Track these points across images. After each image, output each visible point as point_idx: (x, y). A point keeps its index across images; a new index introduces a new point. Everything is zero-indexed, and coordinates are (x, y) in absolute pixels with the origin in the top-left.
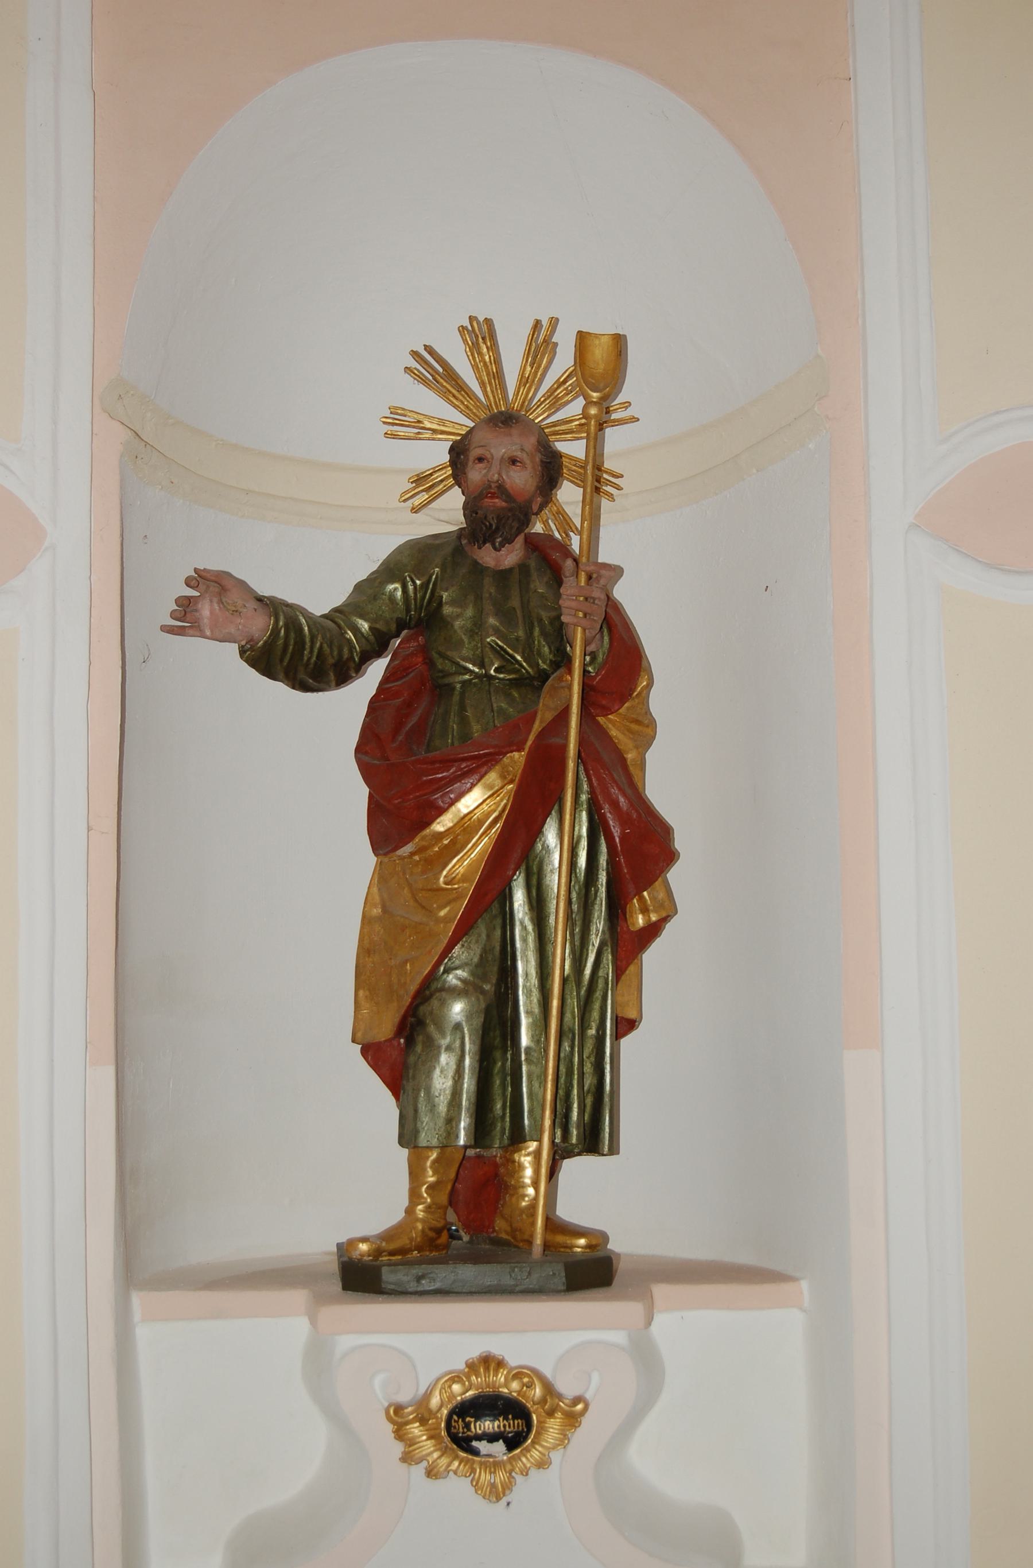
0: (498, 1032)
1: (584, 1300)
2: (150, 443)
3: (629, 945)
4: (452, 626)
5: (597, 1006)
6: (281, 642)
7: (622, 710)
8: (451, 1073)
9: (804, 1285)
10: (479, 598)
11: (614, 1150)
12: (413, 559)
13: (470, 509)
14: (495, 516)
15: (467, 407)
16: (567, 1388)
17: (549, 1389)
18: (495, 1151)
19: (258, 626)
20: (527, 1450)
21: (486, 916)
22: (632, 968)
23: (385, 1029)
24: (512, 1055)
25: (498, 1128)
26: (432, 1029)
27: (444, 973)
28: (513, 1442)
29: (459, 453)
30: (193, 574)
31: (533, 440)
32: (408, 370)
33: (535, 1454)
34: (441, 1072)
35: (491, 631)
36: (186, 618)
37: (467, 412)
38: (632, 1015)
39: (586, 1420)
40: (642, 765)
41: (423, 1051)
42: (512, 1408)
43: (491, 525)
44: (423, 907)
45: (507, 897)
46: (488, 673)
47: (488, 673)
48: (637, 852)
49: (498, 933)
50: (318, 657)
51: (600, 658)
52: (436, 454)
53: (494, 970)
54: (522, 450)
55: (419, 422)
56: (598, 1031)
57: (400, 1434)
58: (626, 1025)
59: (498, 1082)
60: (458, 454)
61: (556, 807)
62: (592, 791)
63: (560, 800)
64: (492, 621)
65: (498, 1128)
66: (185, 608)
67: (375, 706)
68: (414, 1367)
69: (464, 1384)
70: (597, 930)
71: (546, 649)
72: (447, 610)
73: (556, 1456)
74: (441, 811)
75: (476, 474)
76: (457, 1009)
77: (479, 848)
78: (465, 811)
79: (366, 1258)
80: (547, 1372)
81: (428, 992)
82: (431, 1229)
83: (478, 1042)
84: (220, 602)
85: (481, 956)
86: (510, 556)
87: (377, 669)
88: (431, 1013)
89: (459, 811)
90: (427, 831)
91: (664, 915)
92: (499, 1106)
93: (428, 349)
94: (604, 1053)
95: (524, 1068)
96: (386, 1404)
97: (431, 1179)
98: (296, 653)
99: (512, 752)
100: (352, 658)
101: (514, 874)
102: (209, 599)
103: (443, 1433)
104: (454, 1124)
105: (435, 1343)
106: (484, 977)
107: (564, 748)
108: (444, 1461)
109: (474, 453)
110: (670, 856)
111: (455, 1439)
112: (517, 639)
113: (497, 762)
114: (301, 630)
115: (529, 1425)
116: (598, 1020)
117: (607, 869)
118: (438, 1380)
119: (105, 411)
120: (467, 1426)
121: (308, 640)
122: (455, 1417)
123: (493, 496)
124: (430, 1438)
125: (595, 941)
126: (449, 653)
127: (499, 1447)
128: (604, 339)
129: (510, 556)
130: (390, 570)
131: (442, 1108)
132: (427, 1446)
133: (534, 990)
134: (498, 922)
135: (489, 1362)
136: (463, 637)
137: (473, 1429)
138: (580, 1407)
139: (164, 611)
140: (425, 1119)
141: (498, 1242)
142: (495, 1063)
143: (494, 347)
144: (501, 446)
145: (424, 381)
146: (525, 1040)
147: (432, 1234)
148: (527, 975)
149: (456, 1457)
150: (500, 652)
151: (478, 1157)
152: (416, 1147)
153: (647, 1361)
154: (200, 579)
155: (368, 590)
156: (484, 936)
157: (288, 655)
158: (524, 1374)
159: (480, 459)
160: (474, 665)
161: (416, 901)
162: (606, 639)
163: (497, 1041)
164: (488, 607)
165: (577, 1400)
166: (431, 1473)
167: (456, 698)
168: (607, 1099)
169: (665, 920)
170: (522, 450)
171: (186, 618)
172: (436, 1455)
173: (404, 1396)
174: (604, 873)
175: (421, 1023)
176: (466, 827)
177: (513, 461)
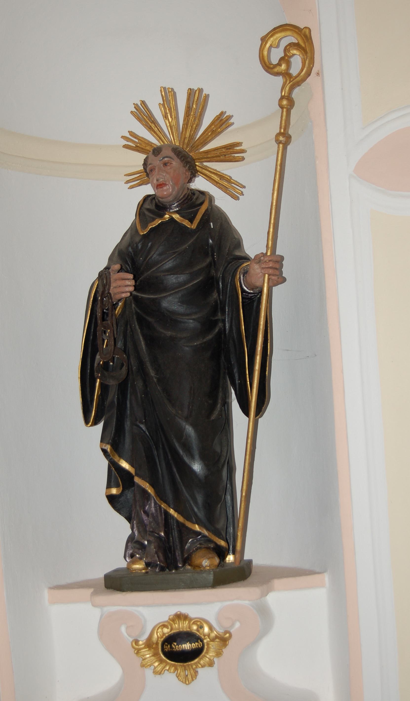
135: (180, 617)
138: (228, 635)
158: (200, 623)
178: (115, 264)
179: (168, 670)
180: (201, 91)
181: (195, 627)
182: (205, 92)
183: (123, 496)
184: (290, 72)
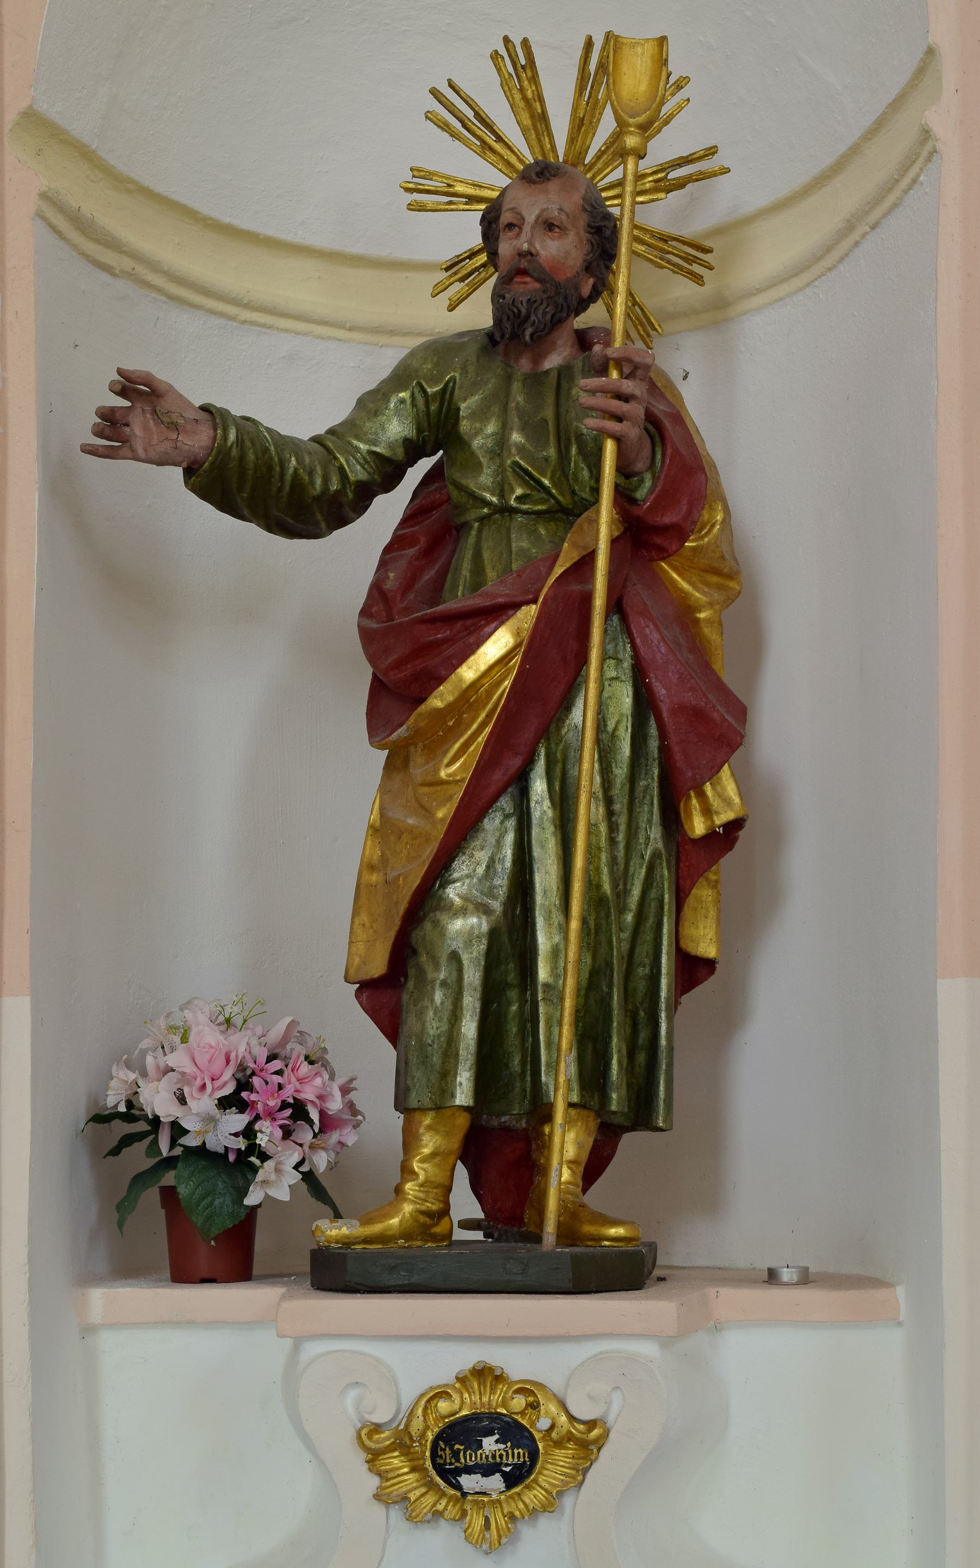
0: (511, 966)
1: (612, 1299)
4: (469, 446)
5: (648, 936)
8: (446, 1016)
9: (900, 1291)
10: (505, 409)
19: (199, 440)
23: (378, 966)
24: (531, 994)
25: (517, 1090)
26: (424, 958)
27: (439, 887)
29: (492, 224)
30: (118, 378)
31: (577, 198)
34: (435, 1013)
35: (514, 450)
41: (415, 988)
42: (513, 1432)
43: (520, 311)
44: (423, 807)
52: (466, 231)
56: (651, 970)
59: (515, 1030)
60: (490, 223)
65: (517, 1090)
66: (111, 423)
74: (441, 680)
88: (424, 939)
89: (461, 680)
90: (423, 708)
92: (517, 1061)
94: (659, 997)
95: (541, 1010)
96: (359, 1425)
98: (263, 485)
102: (135, 413)
103: (428, 1464)
104: (449, 1079)
105: (415, 1352)
106: (491, 894)
108: (430, 1499)
109: (506, 218)
111: (442, 1472)
112: (546, 460)
115: (534, 1455)
117: (660, 758)
118: (422, 1395)
120: (456, 1454)
122: (441, 1443)
124: (413, 1470)
126: (464, 482)
127: (496, 1482)
133: (554, 910)
134: (511, 824)
135: (485, 1375)
136: (482, 460)
137: (463, 1460)
138: (596, 1432)
139: (83, 427)
142: (510, 1003)
144: (532, 205)
146: (543, 974)
150: (524, 475)
159: (510, 226)
160: (492, 494)
161: (417, 801)
163: (512, 977)
164: (515, 420)
167: (472, 540)
172: (418, 1493)
174: (656, 764)
177: (549, 226)
178: (708, 621)
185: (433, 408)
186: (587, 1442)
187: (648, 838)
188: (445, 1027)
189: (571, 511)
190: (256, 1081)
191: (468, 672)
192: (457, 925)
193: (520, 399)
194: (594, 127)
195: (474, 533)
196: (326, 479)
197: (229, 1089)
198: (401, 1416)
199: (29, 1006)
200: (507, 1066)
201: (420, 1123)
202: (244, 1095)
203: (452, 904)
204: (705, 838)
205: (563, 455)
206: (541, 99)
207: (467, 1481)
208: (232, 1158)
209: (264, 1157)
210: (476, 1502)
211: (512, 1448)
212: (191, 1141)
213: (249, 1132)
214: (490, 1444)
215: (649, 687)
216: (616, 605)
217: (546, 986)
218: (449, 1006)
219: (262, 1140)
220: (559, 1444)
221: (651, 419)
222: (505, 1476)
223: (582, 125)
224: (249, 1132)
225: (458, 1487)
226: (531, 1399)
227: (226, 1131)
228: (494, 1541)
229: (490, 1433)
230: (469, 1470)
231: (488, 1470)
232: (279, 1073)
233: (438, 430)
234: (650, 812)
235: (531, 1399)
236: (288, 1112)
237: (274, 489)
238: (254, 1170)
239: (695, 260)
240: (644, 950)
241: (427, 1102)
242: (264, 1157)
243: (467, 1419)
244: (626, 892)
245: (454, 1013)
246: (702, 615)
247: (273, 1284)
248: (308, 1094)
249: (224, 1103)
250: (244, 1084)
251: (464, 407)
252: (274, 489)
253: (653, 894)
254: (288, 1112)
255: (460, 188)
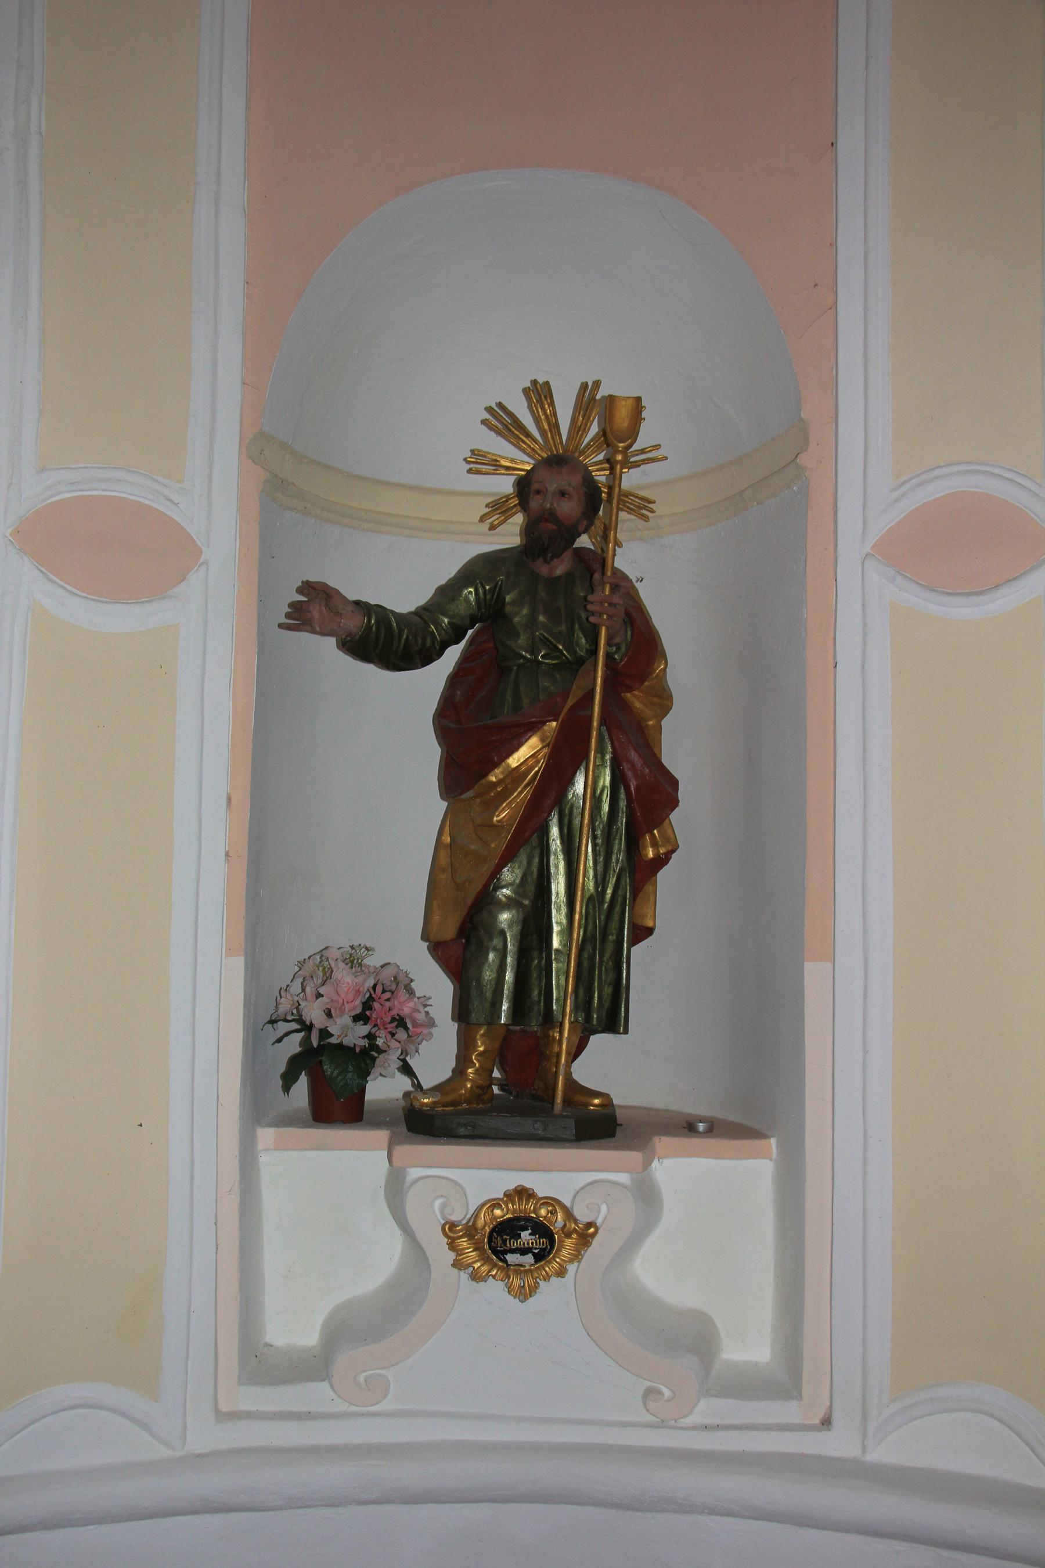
0: (535, 937)
2: (288, 478)
3: (641, 873)
6: (373, 636)
7: (642, 688)
9: (773, 1141)
11: (626, 1032)
12: (476, 571)
13: (528, 530)
14: (546, 537)
15: (533, 450)
16: (582, 1215)
17: (569, 1215)
18: (534, 1026)
19: (354, 623)
20: (550, 1262)
21: (528, 848)
22: (649, 888)
23: (449, 931)
28: (539, 1257)
31: (576, 479)
32: (484, 422)
33: (555, 1265)
36: (299, 618)
37: (531, 453)
38: (650, 924)
39: (596, 1241)
40: (659, 728)
42: (542, 1230)
45: (545, 831)
46: (539, 657)
47: (539, 657)
48: (648, 798)
49: (536, 860)
50: (405, 646)
51: (623, 649)
52: (505, 485)
53: (531, 889)
54: (570, 485)
55: (496, 461)
57: (452, 1245)
58: (642, 933)
61: (584, 764)
62: (614, 752)
63: (587, 757)
64: (541, 618)
67: (454, 680)
68: (465, 1193)
69: (502, 1210)
70: (618, 859)
71: (583, 641)
72: (508, 609)
73: (572, 1268)
74: (496, 765)
75: (535, 503)
76: (505, 917)
77: (522, 795)
78: (514, 765)
79: (425, 1108)
80: (567, 1203)
81: (483, 902)
82: (478, 1087)
83: (516, 944)
84: (327, 605)
85: (522, 878)
86: (561, 567)
87: (453, 654)
89: (509, 766)
90: (483, 781)
91: (670, 848)
92: (536, 993)
93: (500, 405)
97: (481, 1049)
98: (386, 641)
99: (550, 721)
100: (433, 646)
101: (550, 814)
102: (314, 607)
103: (486, 1247)
105: (476, 1178)
106: (524, 895)
107: (591, 717)
108: (485, 1268)
109: (535, 486)
110: (674, 803)
111: (495, 1252)
112: (560, 632)
113: (539, 729)
114: (391, 625)
115: (552, 1241)
116: (615, 928)
118: (483, 1205)
119: (250, 458)
120: (504, 1242)
121: (396, 632)
123: (547, 521)
125: (616, 866)
127: (529, 1259)
128: (630, 402)
129: (561, 567)
130: (467, 575)
131: (489, 995)
132: (472, 1255)
134: (537, 852)
135: (522, 1193)
138: (592, 1230)
140: (476, 1003)
141: (535, 1097)
142: (532, 960)
143: (552, 404)
144: (553, 482)
145: (498, 433)
146: (556, 943)
147: (479, 1091)
148: (557, 894)
149: (495, 1265)
150: (546, 642)
151: (523, 1031)
152: (469, 1024)
153: (648, 1197)
154: (308, 588)
155: (449, 591)
156: (525, 863)
157: (380, 647)
158: (551, 1202)
159: (538, 492)
162: (629, 633)
163: (535, 944)
165: (589, 1225)
166: (476, 1277)
167: (512, 677)
168: (624, 991)
169: (673, 851)
170: (570, 485)
171: (299, 618)
172: (479, 1264)
173: (459, 1215)
175: (475, 928)
176: (516, 776)
177: (563, 494)
178: (653, 726)
179: (494, 1277)
180: (534, 382)
181: (543, 1212)
182: (434, 1030)
183: (453, 1071)
184: (445, 804)
185: (488, 597)
186: (585, 1235)
187: (618, 859)
188: (494, 975)
189: (577, 665)
190: (376, 1005)
191: (514, 761)
192: (505, 916)
193: (543, 594)
194: (586, 431)
195: (514, 673)
196: (424, 639)
197: (358, 1011)
198: (469, 1216)
199: (243, 964)
200: (530, 997)
201: (477, 1032)
202: (367, 1013)
203: (501, 900)
204: (652, 859)
205: (571, 629)
206: (555, 414)
207: (509, 1257)
208: (357, 1050)
209: (380, 1051)
210: (515, 1271)
211: (540, 1238)
212: (333, 1040)
213: (371, 1037)
214: (525, 1235)
215: (622, 772)
216: (603, 721)
217: (557, 950)
218: (497, 962)
219: (380, 1042)
220: (568, 1235)
221: (628, 614)
222: (534, 1254)
223: (578, 429)
224: (371, 1037)
225: (505, 1261)
226: (550, 1208)
227: (355, 1036)
228: (524, 1294)
229: (525, 1229)
230: (512, 1251)
231: (524, 1251)
232: (388, 1000)
233: (492, 614)
234: (620, 846)
235: (550, 1208)
236: (395, 1024)
237: (394, 648)
238: (374, 1059)
239: (645, 508)
240: (614, 925)
241: (482, 1020)
242: (380, 1051)
243: (510, 1219)
244: (604, 891)
245: (498, 966)
246: (651, 723)
247: (381, 1128)
248: (406, 1010)
249: (356, 1019)
250: (367, 1005)
251: (508, 598)
252: (394, 648)
253: (620, 892)
254: (395, 1024)
255: (504, 463)
